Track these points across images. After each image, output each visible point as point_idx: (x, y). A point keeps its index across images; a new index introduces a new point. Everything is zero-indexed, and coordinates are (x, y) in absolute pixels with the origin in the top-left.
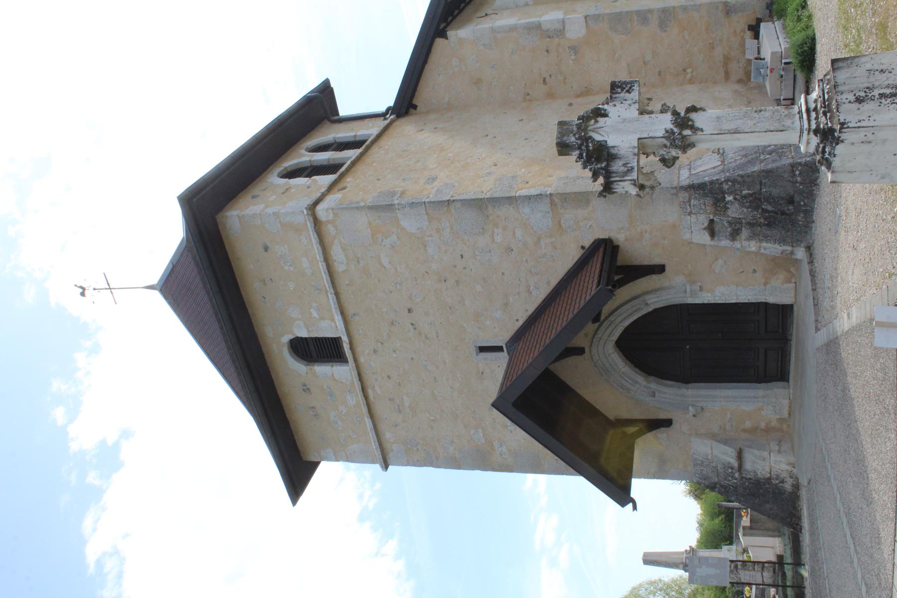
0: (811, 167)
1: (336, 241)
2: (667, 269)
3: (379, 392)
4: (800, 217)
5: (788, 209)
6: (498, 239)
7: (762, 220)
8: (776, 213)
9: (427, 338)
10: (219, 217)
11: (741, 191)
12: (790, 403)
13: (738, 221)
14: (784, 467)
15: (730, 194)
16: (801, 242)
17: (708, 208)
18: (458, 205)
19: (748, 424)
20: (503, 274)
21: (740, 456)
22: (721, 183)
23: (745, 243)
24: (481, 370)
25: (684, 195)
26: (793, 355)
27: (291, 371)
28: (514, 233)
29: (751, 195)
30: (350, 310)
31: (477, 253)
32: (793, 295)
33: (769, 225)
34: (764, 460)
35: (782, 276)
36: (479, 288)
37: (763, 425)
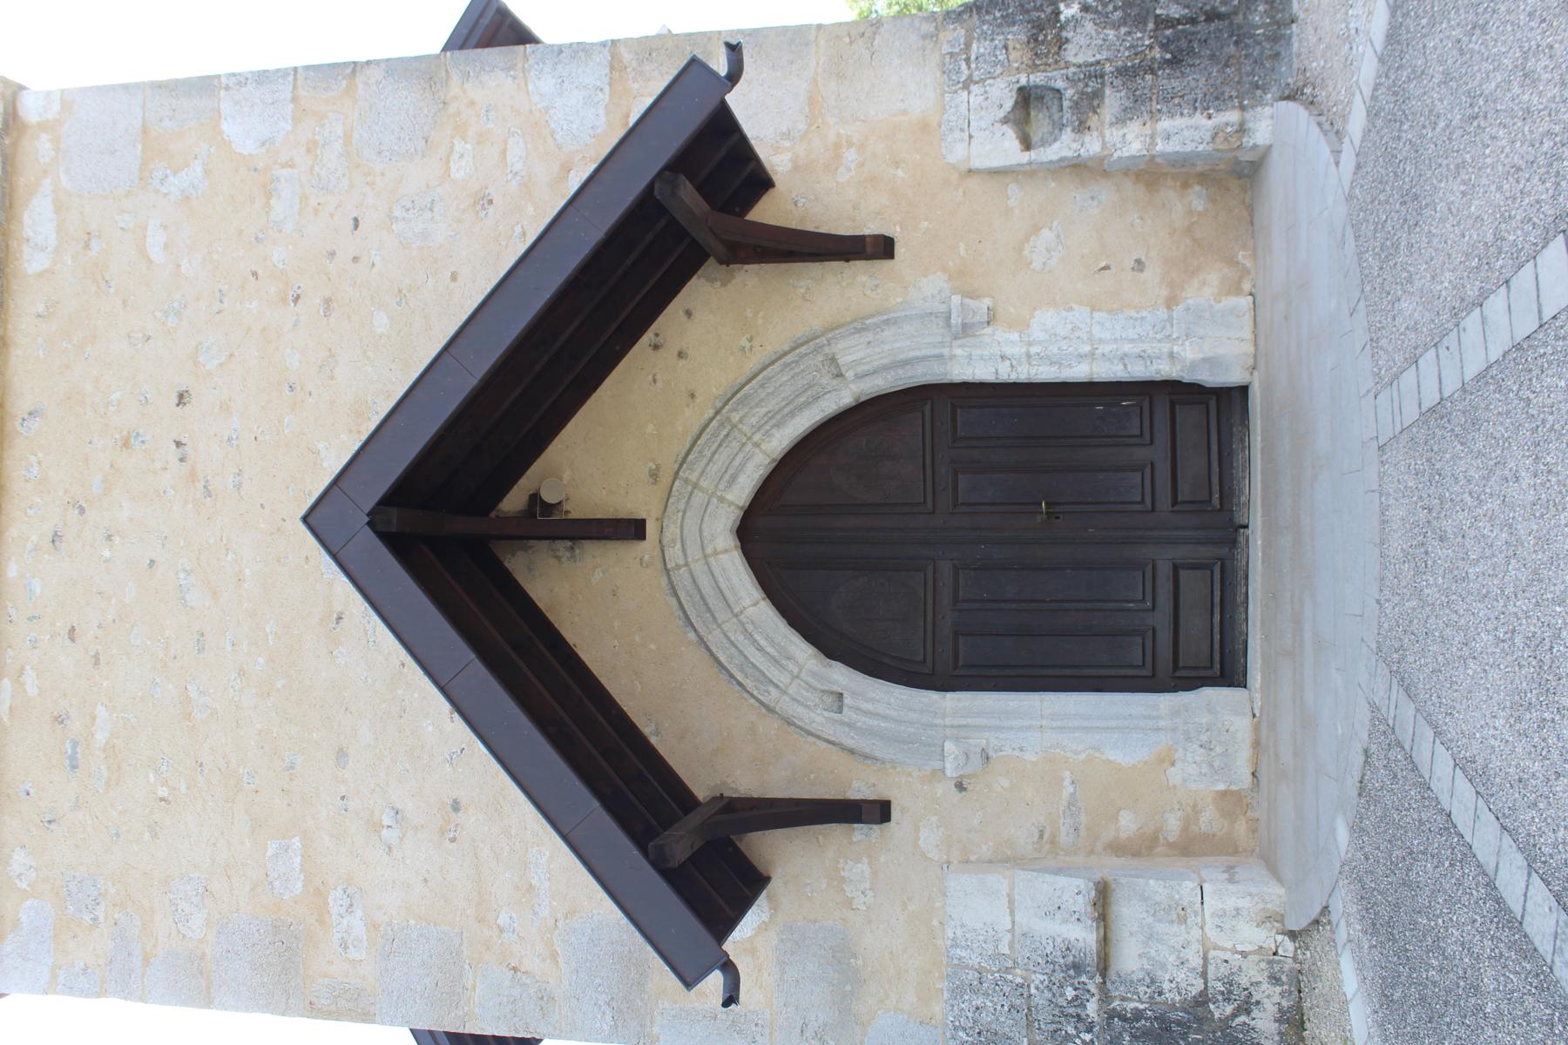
2: (899, 250)
3: (32, 691)
6: (460, 170)
7: (1157, 53)
8: (1193, 21)
9: (208, 493)
12: (1256, 729)
13: (1093, 73)
16: (1264, 89)
18: (376, 74)
19: (1127, 824)
20: (454, 277)
21: (1103, 901)
23: (1112, 135)
24: (338, 607)
25: (957, 33)
26: (1255, 610)
28: (504, 152)
31: (398, 213)
32: (1247, 334)
33: (1175, 62)
34: (1183, 920)
35: (1214, 276)
36: (381, 322)
37: (1173, 825)
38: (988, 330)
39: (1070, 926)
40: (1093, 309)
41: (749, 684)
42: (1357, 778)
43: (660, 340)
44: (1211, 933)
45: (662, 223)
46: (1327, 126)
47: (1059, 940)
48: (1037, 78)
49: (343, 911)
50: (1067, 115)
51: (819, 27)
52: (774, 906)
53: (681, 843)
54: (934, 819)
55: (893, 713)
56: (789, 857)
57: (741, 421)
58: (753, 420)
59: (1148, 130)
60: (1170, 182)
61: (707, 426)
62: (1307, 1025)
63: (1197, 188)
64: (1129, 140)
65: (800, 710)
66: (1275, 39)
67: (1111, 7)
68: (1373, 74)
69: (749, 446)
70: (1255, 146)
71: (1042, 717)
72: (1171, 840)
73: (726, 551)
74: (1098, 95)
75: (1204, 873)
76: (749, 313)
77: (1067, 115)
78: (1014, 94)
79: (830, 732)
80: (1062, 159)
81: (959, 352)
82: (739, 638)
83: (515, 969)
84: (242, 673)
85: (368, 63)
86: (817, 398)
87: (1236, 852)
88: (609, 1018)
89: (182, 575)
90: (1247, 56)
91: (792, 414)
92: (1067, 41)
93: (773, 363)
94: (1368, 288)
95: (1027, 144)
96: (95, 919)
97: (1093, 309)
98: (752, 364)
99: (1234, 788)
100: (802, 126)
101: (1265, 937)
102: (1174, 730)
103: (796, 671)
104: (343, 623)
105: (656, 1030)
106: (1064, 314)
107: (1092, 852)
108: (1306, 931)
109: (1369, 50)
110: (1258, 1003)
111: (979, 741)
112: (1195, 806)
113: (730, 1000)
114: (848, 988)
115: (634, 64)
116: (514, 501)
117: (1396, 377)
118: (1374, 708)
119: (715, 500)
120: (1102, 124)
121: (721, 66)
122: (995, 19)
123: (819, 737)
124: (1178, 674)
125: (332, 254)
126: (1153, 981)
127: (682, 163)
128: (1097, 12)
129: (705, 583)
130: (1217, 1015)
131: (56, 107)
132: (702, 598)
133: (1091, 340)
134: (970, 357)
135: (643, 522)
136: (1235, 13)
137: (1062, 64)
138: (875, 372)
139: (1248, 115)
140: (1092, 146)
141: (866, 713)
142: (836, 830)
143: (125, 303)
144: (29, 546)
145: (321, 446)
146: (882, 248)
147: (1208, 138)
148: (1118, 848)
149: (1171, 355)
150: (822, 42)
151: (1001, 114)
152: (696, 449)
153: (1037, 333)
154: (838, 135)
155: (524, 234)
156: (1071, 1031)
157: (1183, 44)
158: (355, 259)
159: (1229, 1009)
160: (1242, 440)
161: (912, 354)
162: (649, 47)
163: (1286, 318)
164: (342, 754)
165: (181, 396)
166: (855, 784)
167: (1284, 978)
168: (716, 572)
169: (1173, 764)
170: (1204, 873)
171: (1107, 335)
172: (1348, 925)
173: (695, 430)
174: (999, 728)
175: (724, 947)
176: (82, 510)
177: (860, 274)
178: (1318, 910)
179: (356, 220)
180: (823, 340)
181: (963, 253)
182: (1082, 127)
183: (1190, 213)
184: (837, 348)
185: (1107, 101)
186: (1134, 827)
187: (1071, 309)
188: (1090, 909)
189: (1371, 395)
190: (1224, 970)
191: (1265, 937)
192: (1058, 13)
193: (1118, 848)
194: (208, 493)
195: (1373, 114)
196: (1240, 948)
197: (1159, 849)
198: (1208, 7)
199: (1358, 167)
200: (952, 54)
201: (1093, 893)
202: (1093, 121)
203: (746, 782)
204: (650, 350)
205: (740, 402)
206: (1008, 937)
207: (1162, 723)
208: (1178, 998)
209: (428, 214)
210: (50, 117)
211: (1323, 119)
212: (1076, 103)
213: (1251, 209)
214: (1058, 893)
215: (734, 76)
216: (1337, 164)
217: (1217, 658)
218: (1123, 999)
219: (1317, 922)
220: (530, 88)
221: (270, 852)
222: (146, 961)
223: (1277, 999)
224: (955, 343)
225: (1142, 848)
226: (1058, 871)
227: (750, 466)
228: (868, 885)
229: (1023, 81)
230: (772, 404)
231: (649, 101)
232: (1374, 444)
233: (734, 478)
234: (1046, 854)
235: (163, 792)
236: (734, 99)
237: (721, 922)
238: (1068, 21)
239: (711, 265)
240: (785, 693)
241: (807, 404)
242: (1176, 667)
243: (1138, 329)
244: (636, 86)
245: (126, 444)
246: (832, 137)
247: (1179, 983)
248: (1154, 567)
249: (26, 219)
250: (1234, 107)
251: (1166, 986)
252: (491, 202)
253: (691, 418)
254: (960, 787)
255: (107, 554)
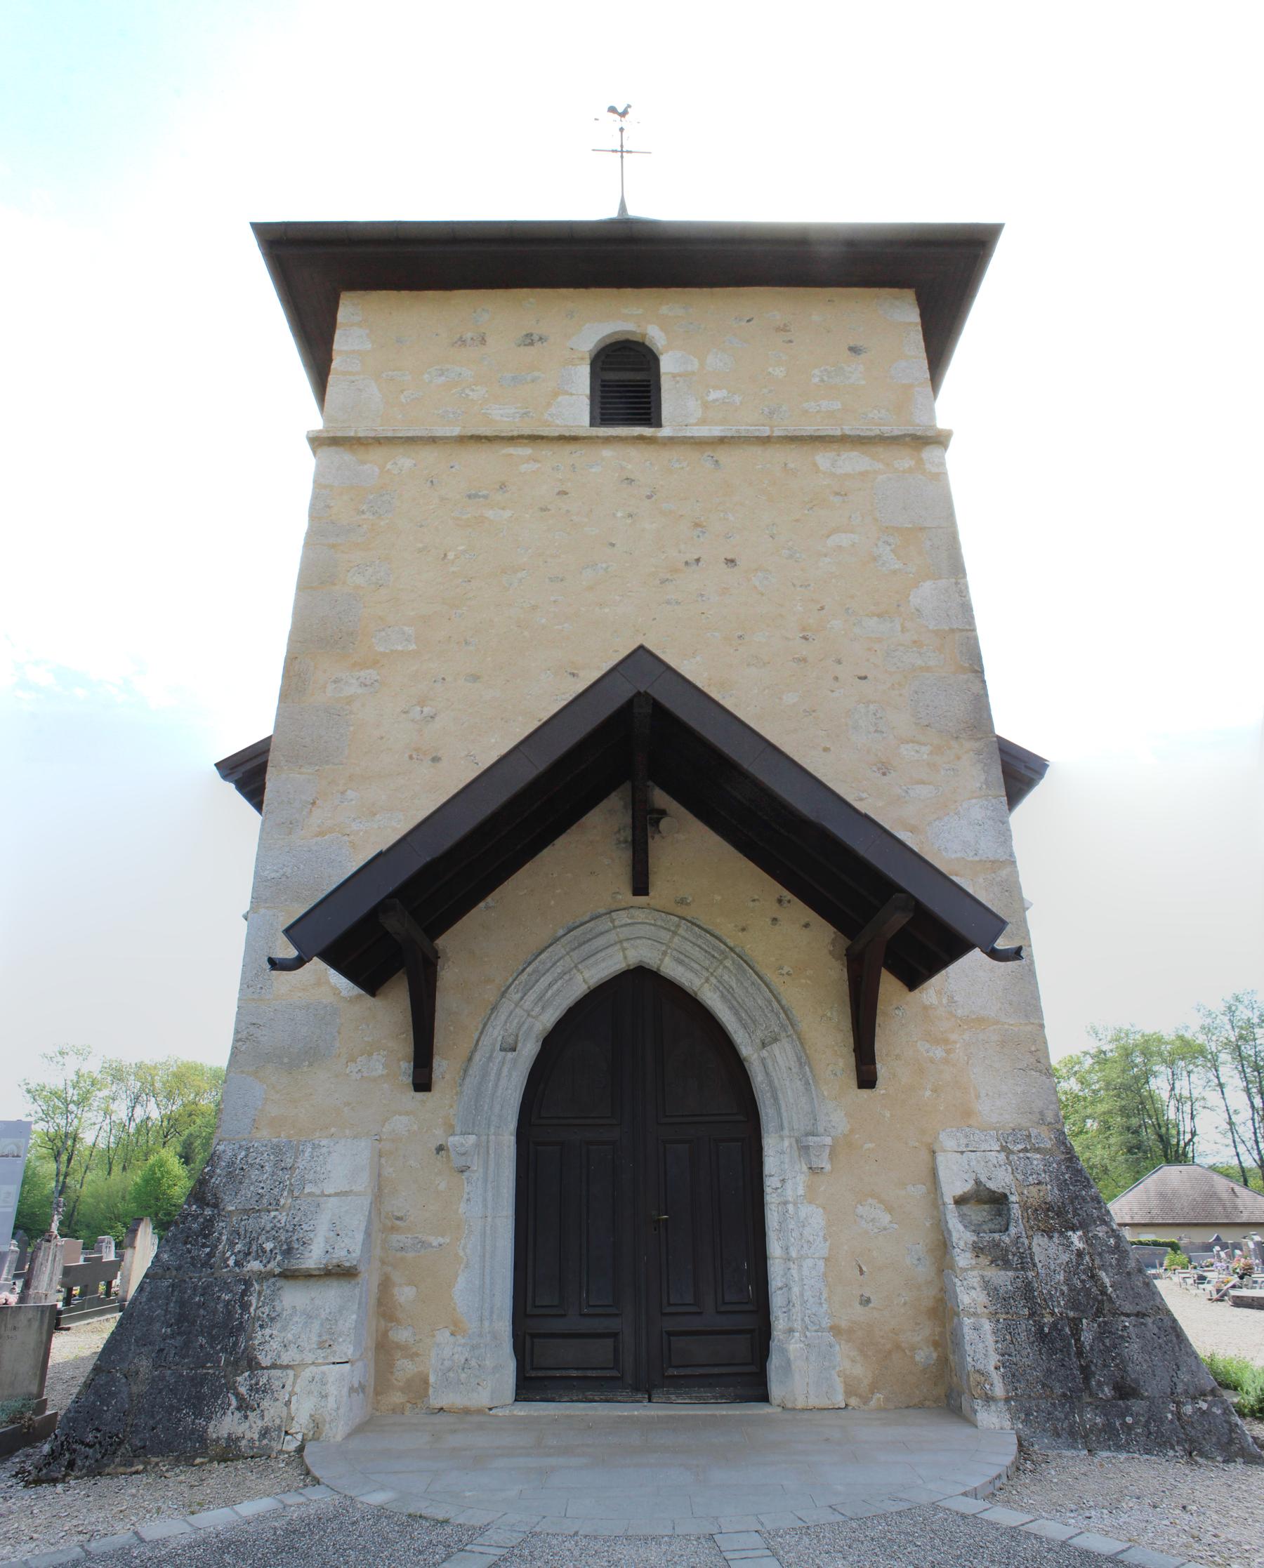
0: (1231, 1442)
1: (881, 466)
2: (865, 1093)
4: (1090, 1417)
5: (1100, 1384)
6: (907, 751)
7: (1048, 1319)
8: (1080, 1354)
9: (663, 582)
10: (909, 295)
11: (1102, 1267)
12: (480, 1412)
13: (1025, 1261)
14: (303, 1411)
15: (1086, 1239)
16: (1026, 1422)
17: (1034, 1190)
19: (405, 1294)
20: (826, 750)
21: (341, 1273)
22: (1105, 1223)
23: (974, 1278)
24: (581, 674)
27: (592, 319)
28: (923, 783)
29: (1103, 1292)
30: (730, 459)
32: (813, 1402)
34: (321, 1346)
35: (859, 1370)
36: (790, 698)
37: (402, 1335)
38: (805, 1168)
39: (322, 1245)
40: (826, 1259)
41: (524, 977)
42: (424, 1513)
43: (786, 904)
44: (307, 1373)
45: (639, 376)
46: (998, 1484)
47: (312, 1236)
48: (1016, 1211)
49: (362, 679)
50: (987, 1237)
51: (1042, 1026)
52: (353, 1000)
53: (395, 924)
54: (415, 1127)
55: (500, 1092)
56: (388, 1014)
57: (725, 967)
58: (726, 977)
59: (980, 1310)
60: (938, 1330)
61: (721, 941)
62: (223, 1465)
63: (935, 1355)
64: (971, 1292)
65: (503, 1018)
66: (1072, 1433)
67: (1084, 1277)
68: (1050, 1535)
69: (706, 974)
70: (975, 1411)
71: (494, 1217)
72: (390, 1334)
73: (625, 958)
74: (1007, 1265)
75: (360, 1364)
76: (809, 972)
77: (987, 1237)
78: (1001, 1190)
79: (486, 1041)
80: (949, 1232)
81: (786, 1143)
82: (558, 969)
83: (314, 803)
84: (534, 608)
85: (984, 682)
86: (745, 1027)
87: (377, 1393)
88: (273, 875)
89: (604, 565)
90: (1053, 1405)
91: (732, 1008)
92: (1051, 1238)
93: (771, 991)
94: (854, 1525)
95: (960, 1201)
96: (363, 512)
97: (826, 1259)
98: (769, 975)
99: (431, 1391)
100: (960, 1012)
101: (301, 1424)
102: (480, 1335)
103: (533, 1013)
104: (570, 678)
105: (262, 911)
106: (821, 1234)
107: (383, 1262)
108: (303, 1463)
109: (1071, 1531)
110: (246, 1417)
111: (476, 1164)
112: (417, 1355)
113: (275, 964)
114: (286, 1060)
115: (998, 879)
116: (660, 798)
117: (775, 1554)
118: (483, 1529)
119: (664, 948)
120: (983, 1269)
121: (1001, 944)
122: (1063, 1174)
123: (481, 1033)
124: (528, 1338)
125: (839, 662)
126: (272, 1319)
127: (922, 914)
128: (1078, 1264)
129: (601, 941)
130: (239, 1379)
131: (934, 470)
132: (589, 940)
133: (802, 1257)
134: (782, 1153)
135: (647, 894)
136: (1091, 1395)
137: (1030, 1233)
138: (767, 1074)
139: (1001, 1404)
140: (963, 1259)
141: (500, 1070)
142: (409, 1049)
143: (797, 521)
144: (624, 464)
145: (698, 658)
146: (867, 1080)
147: (979, 1366)
148: (385, 1285)
149: (791, 1330)
150: (1029, 1028)
151: (983, 1179)
152: (703, 933)
153: (804, 1210)
154: (955, 1042)
155: (861, 800)
156: (238, 1247)
157: (1059, 1345)
158: (836, 679)
159: (243, 1390)
160: (722, 1396)
161: (782, 1103)
162: (1012, 888)
163: (827, 1440)
164: (475, 678)
165: (732, 561)
166: (445, 1063)
167: (265, 1442)
168: (609, 951)
169: (452, 1334)
170: (360, 1364)
171: (805, 1272)
172: (299, 1505)
173: (717, 932)
174: (485, 1181)
175: (315, 958)
176: (649, 497)
177: (841, 1061)
178: (317, 1473)
179: (865, 678)
180: (791, 1032)
181: (868, 1146)
182: (978, 1250)
183: (913, 1349)
184: (785, 1042)
185: (1003, 1273)
186: (402, 1299)
187: (825, 1240)
188: (335, 1261)
189: (759, 1528)
190: (276, 1384)
191: (301, 1424)
192: (1074, 1229)
193: (385, 1285)
194: (663, 582)
195: (1014, 1533)
196: (294, 1399)
197: (383, 1323)
198: (1093, 1368)
199: (964, 1517)
200: (1029, 1136)
201: (348, 1264)
202: (984, 1260)
203: (448, 976)
204: (777, 896)
205: (740, 967)
206: (318, 1192)
207: (486, 1323)
208: (256, 1342)
209: (872, 729)
210: (928, 466)
211: (1004, 1480)
212: (998, 1245)
213: (920, 1406)
214: (350, 1234)
215: (995, 954)
216: (965, 1494)
217: (541, 1374)
218: (260, 1293)
219: (308, 1473)
220: (974, 801)
221: (406, 629)
222: (333, 546)
223: (248, 1435)
224: (793, 1140)
225: (385, 1309)
226: (368, 1234)
227: (690, 975)
228: (365, 1074)
229: (1013, 1198)
230: (739, 991)
231: (971, 891)
232: (715, 1530)
233: (681, 962)
234: (384, 1222)
235: (451, 556)
236: (976, 955)
237: (337, 956)
238: (1068, 1238)
239: (844, 942)
240: (517, 1005)
241: (740, 1020)
242: (533, 1336)
243: (811, 1300)
244: (981, 880)
245: (697, 525)
246: (954, 1037)
247: (270, 1344)
248: (617, 1315)
249: (854, 454)
250: (1007, 1392)
251: (267, 1331)
252: (884, 774)
253: (726, 928)
254: (440, 1149)
255: (619, 514)
